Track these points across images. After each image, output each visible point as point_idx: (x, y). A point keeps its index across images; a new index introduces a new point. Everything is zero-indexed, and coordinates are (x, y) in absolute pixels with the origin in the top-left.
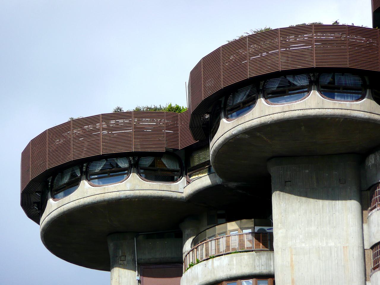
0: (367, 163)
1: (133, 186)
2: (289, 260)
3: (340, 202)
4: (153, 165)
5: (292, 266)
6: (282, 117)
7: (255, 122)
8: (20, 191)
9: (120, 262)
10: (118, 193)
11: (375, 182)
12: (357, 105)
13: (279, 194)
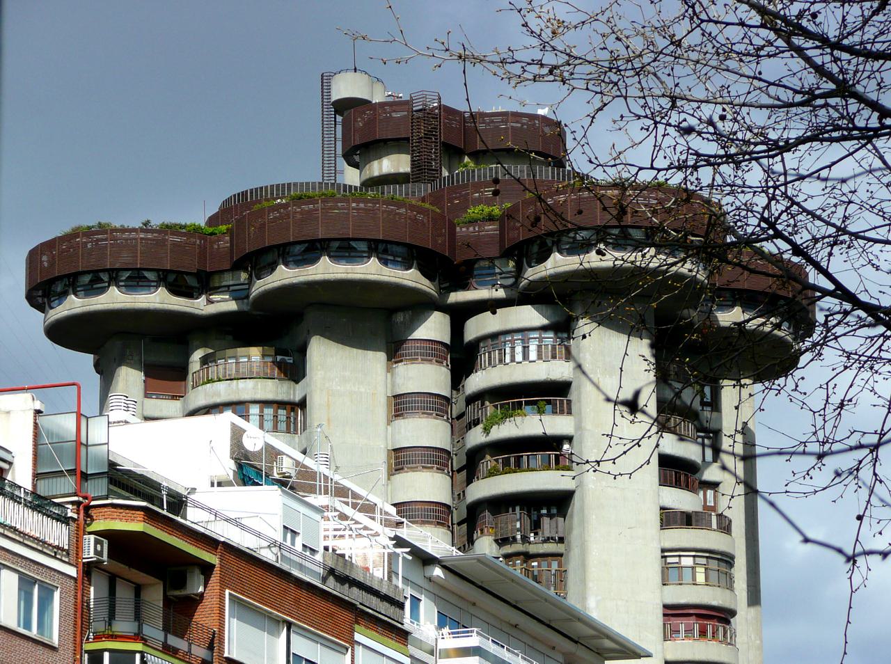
0: (394, 316)
1: (158, 299)
2: (326, 400)
3: (371, 352)
4: (176, 280)
5: (328, 405)
6: (346, 277)
7: (319, 277)
8: (594, 571)
9: (128, 361)
10: (148, 304)
11: (404, 338)
12: (407, 274)
13: (320, 340)
